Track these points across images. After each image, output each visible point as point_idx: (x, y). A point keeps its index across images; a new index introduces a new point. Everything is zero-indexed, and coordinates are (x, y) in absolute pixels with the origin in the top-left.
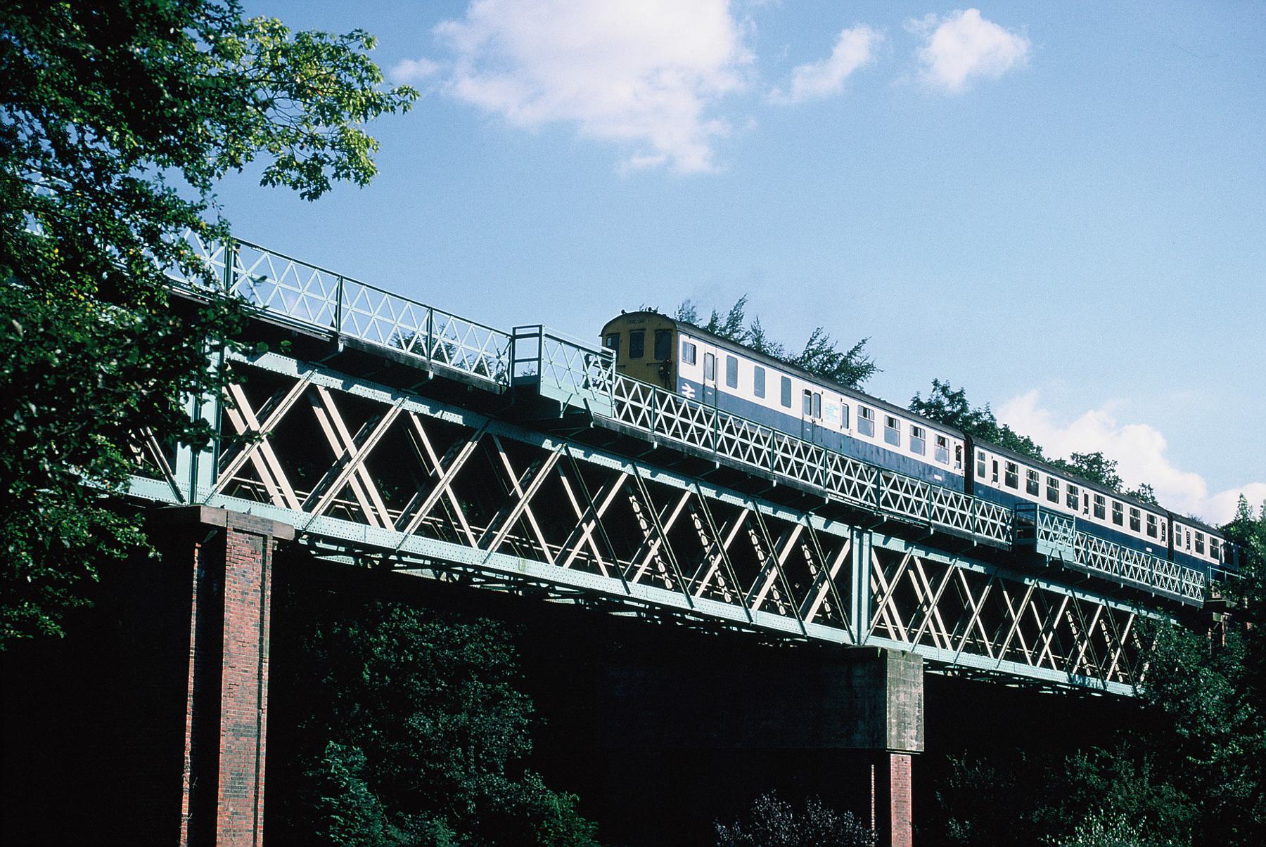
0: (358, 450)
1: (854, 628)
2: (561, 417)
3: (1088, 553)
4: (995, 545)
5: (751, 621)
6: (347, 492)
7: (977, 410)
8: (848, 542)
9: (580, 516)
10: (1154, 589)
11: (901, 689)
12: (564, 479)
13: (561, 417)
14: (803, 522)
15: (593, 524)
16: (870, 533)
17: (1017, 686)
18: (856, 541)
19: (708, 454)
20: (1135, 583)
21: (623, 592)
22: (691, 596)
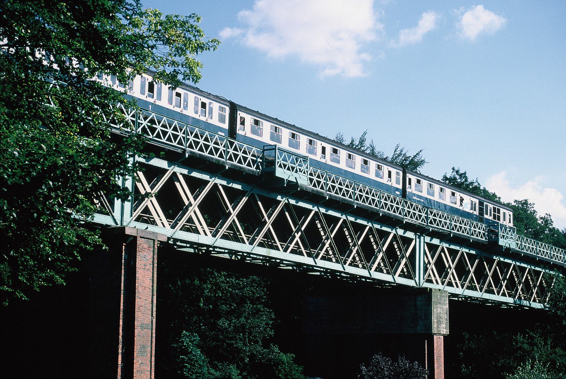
0: (195, 201)
1: (417, 279)
2: (285, 185)
3: (522, 245)
4: (480, 242)
5: (371, 276)
6: (190, 220)
7: (472, 181)
8: (414, 240)
9: (501, 278)
10: (552, 260)
11: (438, 306)
12: (287, 213)
13: (285, 185)
14: (394, 231)
15: (300, 233)
16: (424, 237)
17: (491, 304)
18: (418, 240)
19: (351, 201)
20: (543, 258)
21: (313, 264)
22: (344, 265)
